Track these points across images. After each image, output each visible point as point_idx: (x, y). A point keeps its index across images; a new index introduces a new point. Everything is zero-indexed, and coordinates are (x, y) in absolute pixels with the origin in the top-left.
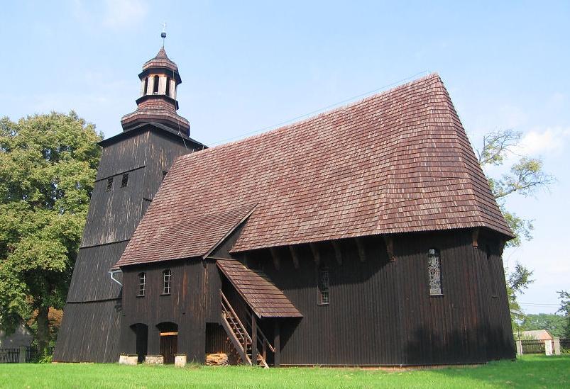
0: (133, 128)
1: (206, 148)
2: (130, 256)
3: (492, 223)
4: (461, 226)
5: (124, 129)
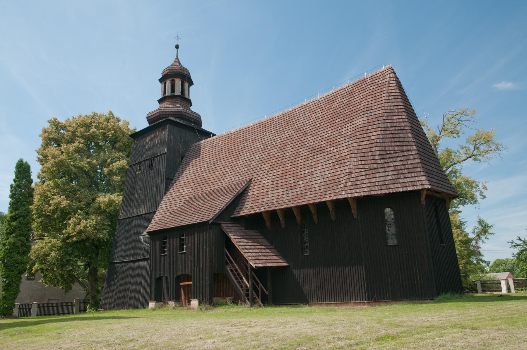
0: (157, 122)
1: (214, 135)
2: (154, 225)
3: (437, 185)
4: (410, 189)
5: (149, 123)
